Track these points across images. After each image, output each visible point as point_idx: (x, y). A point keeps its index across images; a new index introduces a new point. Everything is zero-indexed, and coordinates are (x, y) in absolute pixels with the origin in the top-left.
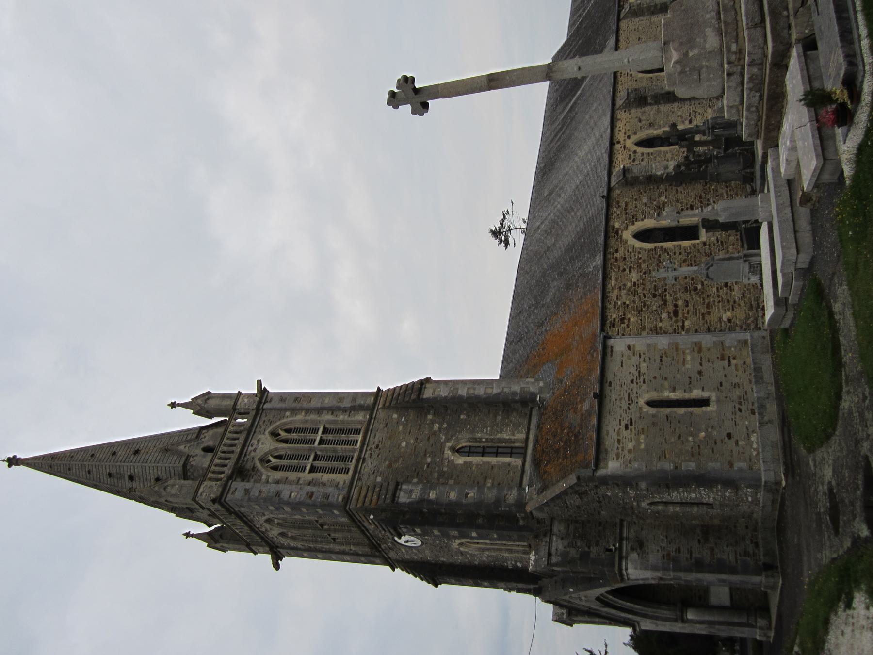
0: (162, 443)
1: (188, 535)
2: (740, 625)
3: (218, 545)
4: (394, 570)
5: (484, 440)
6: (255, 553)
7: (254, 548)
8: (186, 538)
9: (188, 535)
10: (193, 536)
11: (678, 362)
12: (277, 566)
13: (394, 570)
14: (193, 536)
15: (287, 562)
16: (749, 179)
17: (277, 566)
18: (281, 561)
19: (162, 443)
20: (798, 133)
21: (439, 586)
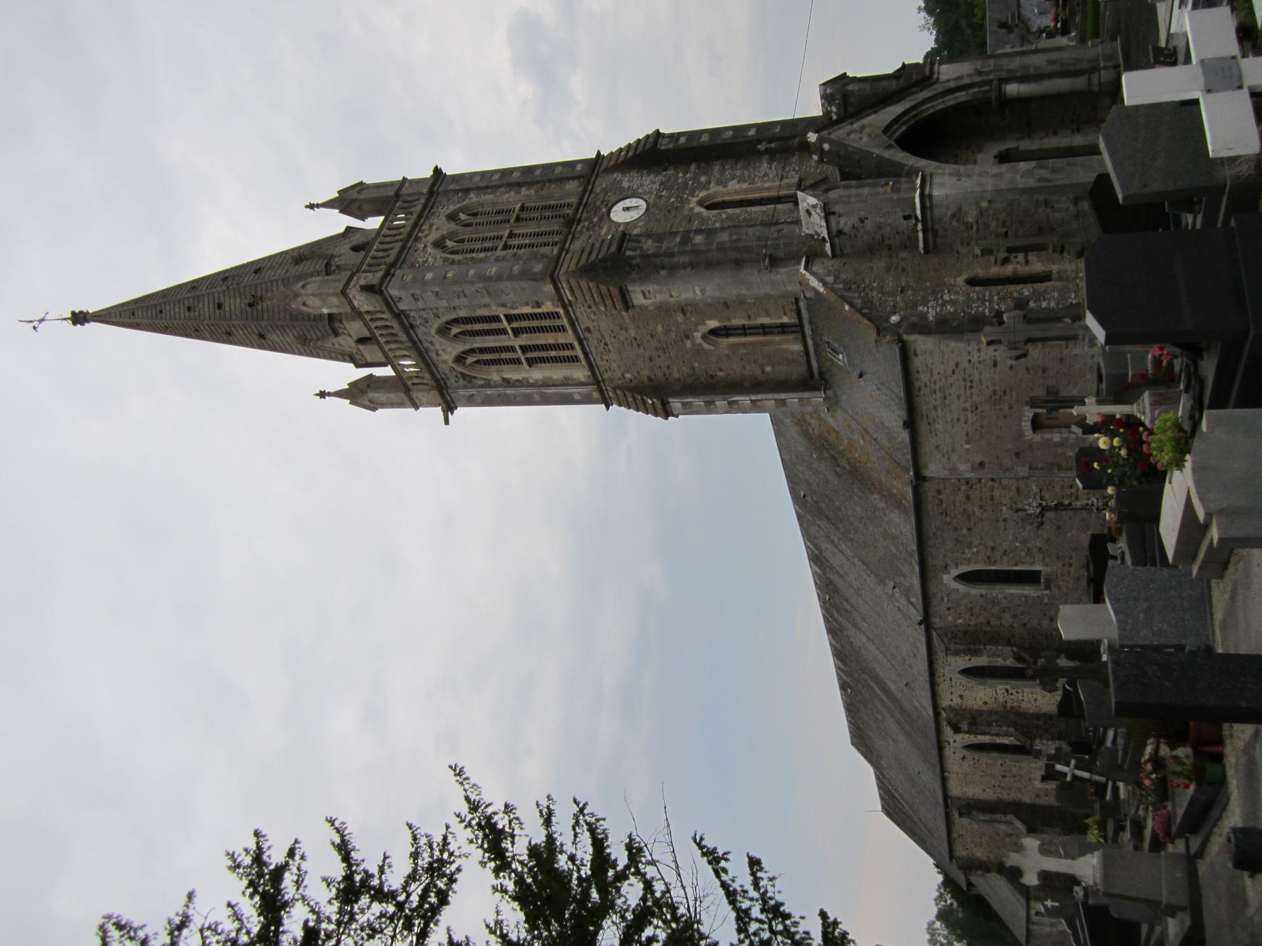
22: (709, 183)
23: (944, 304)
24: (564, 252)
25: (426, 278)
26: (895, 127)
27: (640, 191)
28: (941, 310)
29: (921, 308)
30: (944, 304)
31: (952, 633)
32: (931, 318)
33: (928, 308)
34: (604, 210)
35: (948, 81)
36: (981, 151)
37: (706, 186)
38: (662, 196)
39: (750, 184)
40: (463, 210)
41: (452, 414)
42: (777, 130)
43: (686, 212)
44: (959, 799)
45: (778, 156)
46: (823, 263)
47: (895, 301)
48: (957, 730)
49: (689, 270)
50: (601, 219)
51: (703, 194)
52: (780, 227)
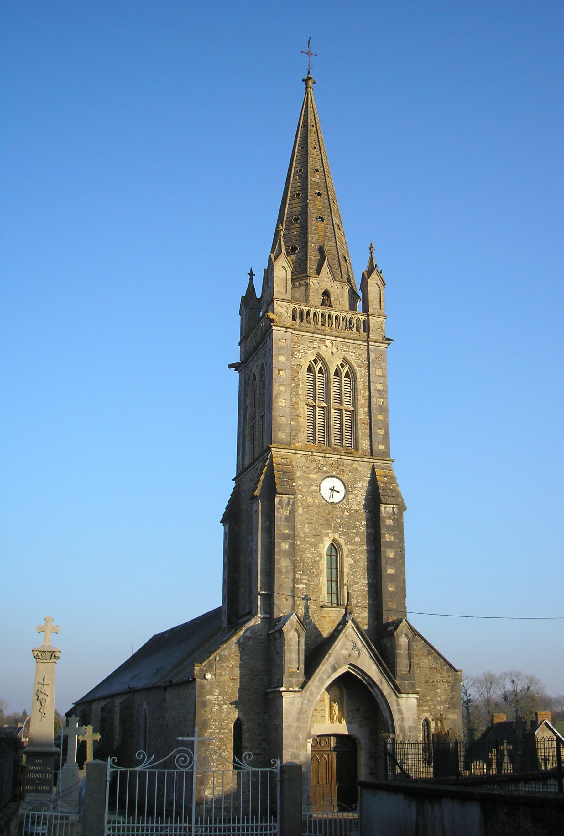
0: (329, 182)
1: (251, 274)
2: (292, 268)
3: (243, 308)
4: (233, 480)
5: (277, 623)
6: (240, 344)
7: (243, 343)
8: (248, 274)
9: (251, 274)
10: (251, 279)
11: (435, 673)
12: (230, 366)
13: (233, 480)
14: (251, 279)
15: (235, 376)
16: (531, 679)
17: (230, 366)
18: (235, 370)
19: (329, 182)
20: (226, 707)
21: (222, 524)
22: (353, 544)
23: (220, 706)
24: (294, 451)
25: (280, 356)
26: (380, 668)
27: (350, 496)
28: (214, 704)
29: (217, 691)
30: (220, 706)
31: (131, 707)
32: (208, 697)
33: (217, 696)
34: (334, 473)
35: (398, 705)
36: (361, 726)
37: (350, 542)
38: (344, 512)
39: (348, 573)
40: (351, 367)
41: (235, 370)
42: (389, 588)
43: (325, 532)
44: (91, 710)
45: (373, 590)
46: (264, 628)
47: (225, 675)
48: (103, 709)
49: (268, 540)
50: (325, 472)
51: (342, 541)
52: (290, 599)
